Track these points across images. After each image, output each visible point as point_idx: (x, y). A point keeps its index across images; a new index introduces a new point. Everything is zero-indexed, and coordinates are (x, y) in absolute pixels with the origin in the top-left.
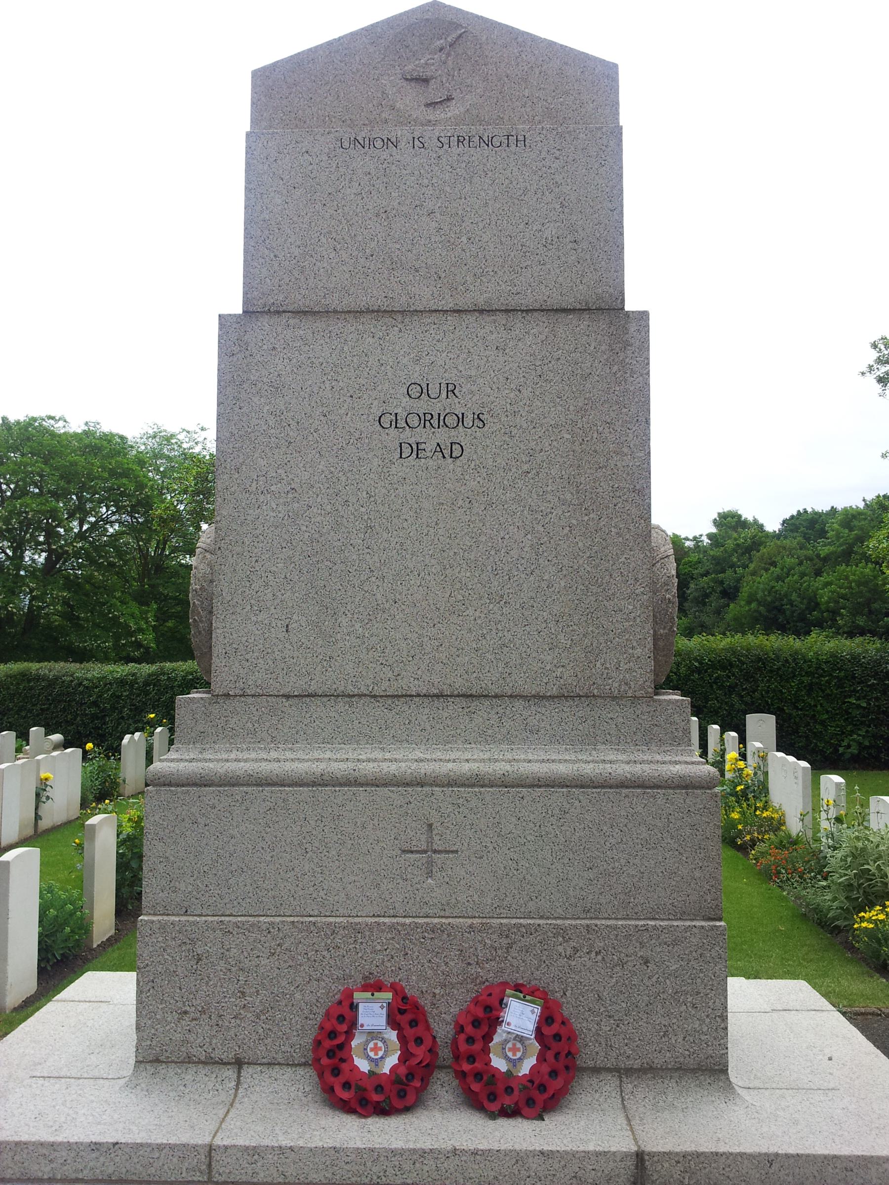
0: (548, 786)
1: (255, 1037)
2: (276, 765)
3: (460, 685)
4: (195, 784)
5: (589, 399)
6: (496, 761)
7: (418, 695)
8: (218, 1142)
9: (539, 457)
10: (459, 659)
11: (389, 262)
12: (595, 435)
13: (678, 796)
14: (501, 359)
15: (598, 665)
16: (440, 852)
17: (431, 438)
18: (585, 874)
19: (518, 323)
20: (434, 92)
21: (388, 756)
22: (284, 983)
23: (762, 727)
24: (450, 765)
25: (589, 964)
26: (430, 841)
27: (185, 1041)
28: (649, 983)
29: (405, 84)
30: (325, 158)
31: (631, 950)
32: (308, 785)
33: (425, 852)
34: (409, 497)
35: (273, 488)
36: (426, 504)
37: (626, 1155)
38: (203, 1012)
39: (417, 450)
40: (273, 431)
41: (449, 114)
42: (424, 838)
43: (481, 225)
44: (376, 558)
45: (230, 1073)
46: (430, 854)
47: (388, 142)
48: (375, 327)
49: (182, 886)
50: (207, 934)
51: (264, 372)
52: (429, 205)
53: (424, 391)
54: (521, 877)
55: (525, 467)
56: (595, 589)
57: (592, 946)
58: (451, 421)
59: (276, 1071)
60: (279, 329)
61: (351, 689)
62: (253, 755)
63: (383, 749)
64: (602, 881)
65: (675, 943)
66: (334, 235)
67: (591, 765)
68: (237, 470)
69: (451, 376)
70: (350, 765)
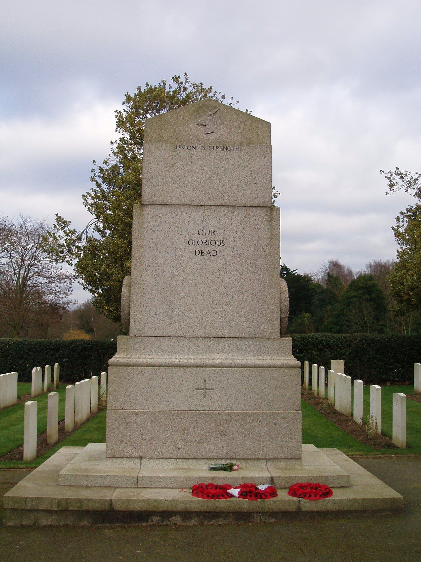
0: (244, 367)
1: (146, 449)
2: (153, 360)
3: (215, 334)
4: (125, 366)
5: (260, 237)
6: (227, 359)
7: (201, 337)
8: (140, 475)
9: (243, 256)
10: (215, 325)
11: (192, 188)
12: (262, 249)
13: (287, 370)
14: (231, 222)
15: (262, 327)
16: (208, 389)
17: (207, 249)
18: (256, 396)
19: (236, 211)
20: (208, 129)
21: (190, 357)
22: (156, 431)
23: (337, 366)
24: (212, 361)
25: (257, 425)
26: (205, 386)
27: (123, 451)
28: (276, 431)
29: (198, 126)
30: (171, 152)
31: (271, 420)
32: (163, 366)
33: (203, 389)
34: (198, 269)
35: (151, 265)
36: (204, 272)
37: (268, 477)
38: (129, 441)
39: (201, 252)
40: (151, 245)
41: (213, 138)
42: (203, 384)
43: (224, 177)
44: (187, 290)
45: (138, 461)
46: (205, 390)
47: (192, 147)
48: (187, 210)
49: (121, 400)
50: (130, 415)
51: (149, 225)
52: (206, 169)
53: (204, 232)
54: (235, 397)
55: (238, 259)
56: (261, 301)
57: (258, 419)
58: (213, 243)
59: (153, 460)
60: (154, 210)
61: (178, 335)
62: (144, 357)
63: (189, 355)
64: (262, 398)
65: (285, 418)
66: (174, 178)
67: (259, 361)
68: (139, 258)
69: (213, 228)
70: (178, 360)
